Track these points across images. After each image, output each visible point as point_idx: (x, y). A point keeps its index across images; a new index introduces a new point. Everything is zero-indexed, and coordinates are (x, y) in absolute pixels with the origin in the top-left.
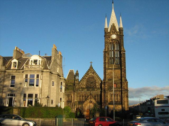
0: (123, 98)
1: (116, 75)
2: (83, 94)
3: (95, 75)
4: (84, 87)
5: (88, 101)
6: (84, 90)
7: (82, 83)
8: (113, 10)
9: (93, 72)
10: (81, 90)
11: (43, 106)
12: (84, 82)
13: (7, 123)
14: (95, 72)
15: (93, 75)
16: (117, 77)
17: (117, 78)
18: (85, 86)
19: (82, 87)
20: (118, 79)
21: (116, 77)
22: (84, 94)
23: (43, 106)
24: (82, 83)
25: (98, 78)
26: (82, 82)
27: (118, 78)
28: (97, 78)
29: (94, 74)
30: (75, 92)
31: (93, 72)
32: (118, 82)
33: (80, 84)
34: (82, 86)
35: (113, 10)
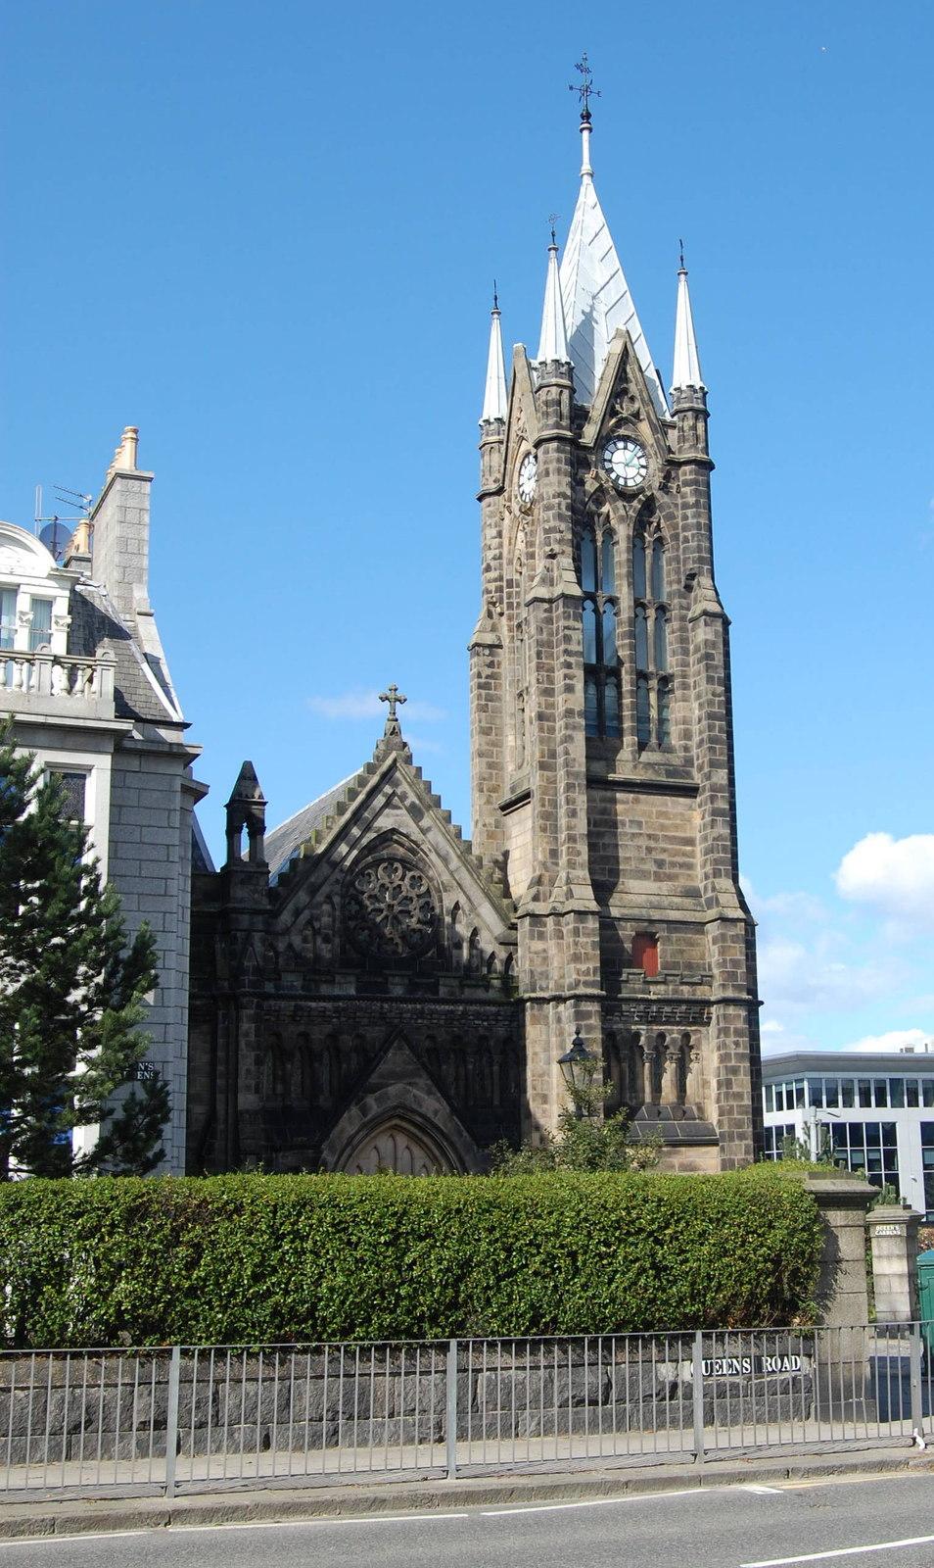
0: (740, 1057)
1: (649, 850)
2: (318, 1033)
3: (436, 837)
4: (326, 950)
5: (370, 1100)
6: (325, 990)
7: (297, 913)
8: (588, 194)
9: (412, 798)
10: (293, 980)
11: (72, 990)
12: (319, 898)
13: (188, 749)
14: (437, 801)
15: (416, 835)
16: (660, 864)
17: (658, 878)
18: (327, 940)
19: (297, 957)
20: (665, 887)
21: (651, 867)
22: (328, 1029)
23: (72, 990)
24: (305, 916)
25: (465, 863)
26: (302, 897)
27: (670, 878)
28: (455, 863)
29: (426, 822)
30: (239, 1007)
31: (412, 798)
32: (420, 1119)
33: (286, 917)
34: (297, 940)
35: (588, 194)
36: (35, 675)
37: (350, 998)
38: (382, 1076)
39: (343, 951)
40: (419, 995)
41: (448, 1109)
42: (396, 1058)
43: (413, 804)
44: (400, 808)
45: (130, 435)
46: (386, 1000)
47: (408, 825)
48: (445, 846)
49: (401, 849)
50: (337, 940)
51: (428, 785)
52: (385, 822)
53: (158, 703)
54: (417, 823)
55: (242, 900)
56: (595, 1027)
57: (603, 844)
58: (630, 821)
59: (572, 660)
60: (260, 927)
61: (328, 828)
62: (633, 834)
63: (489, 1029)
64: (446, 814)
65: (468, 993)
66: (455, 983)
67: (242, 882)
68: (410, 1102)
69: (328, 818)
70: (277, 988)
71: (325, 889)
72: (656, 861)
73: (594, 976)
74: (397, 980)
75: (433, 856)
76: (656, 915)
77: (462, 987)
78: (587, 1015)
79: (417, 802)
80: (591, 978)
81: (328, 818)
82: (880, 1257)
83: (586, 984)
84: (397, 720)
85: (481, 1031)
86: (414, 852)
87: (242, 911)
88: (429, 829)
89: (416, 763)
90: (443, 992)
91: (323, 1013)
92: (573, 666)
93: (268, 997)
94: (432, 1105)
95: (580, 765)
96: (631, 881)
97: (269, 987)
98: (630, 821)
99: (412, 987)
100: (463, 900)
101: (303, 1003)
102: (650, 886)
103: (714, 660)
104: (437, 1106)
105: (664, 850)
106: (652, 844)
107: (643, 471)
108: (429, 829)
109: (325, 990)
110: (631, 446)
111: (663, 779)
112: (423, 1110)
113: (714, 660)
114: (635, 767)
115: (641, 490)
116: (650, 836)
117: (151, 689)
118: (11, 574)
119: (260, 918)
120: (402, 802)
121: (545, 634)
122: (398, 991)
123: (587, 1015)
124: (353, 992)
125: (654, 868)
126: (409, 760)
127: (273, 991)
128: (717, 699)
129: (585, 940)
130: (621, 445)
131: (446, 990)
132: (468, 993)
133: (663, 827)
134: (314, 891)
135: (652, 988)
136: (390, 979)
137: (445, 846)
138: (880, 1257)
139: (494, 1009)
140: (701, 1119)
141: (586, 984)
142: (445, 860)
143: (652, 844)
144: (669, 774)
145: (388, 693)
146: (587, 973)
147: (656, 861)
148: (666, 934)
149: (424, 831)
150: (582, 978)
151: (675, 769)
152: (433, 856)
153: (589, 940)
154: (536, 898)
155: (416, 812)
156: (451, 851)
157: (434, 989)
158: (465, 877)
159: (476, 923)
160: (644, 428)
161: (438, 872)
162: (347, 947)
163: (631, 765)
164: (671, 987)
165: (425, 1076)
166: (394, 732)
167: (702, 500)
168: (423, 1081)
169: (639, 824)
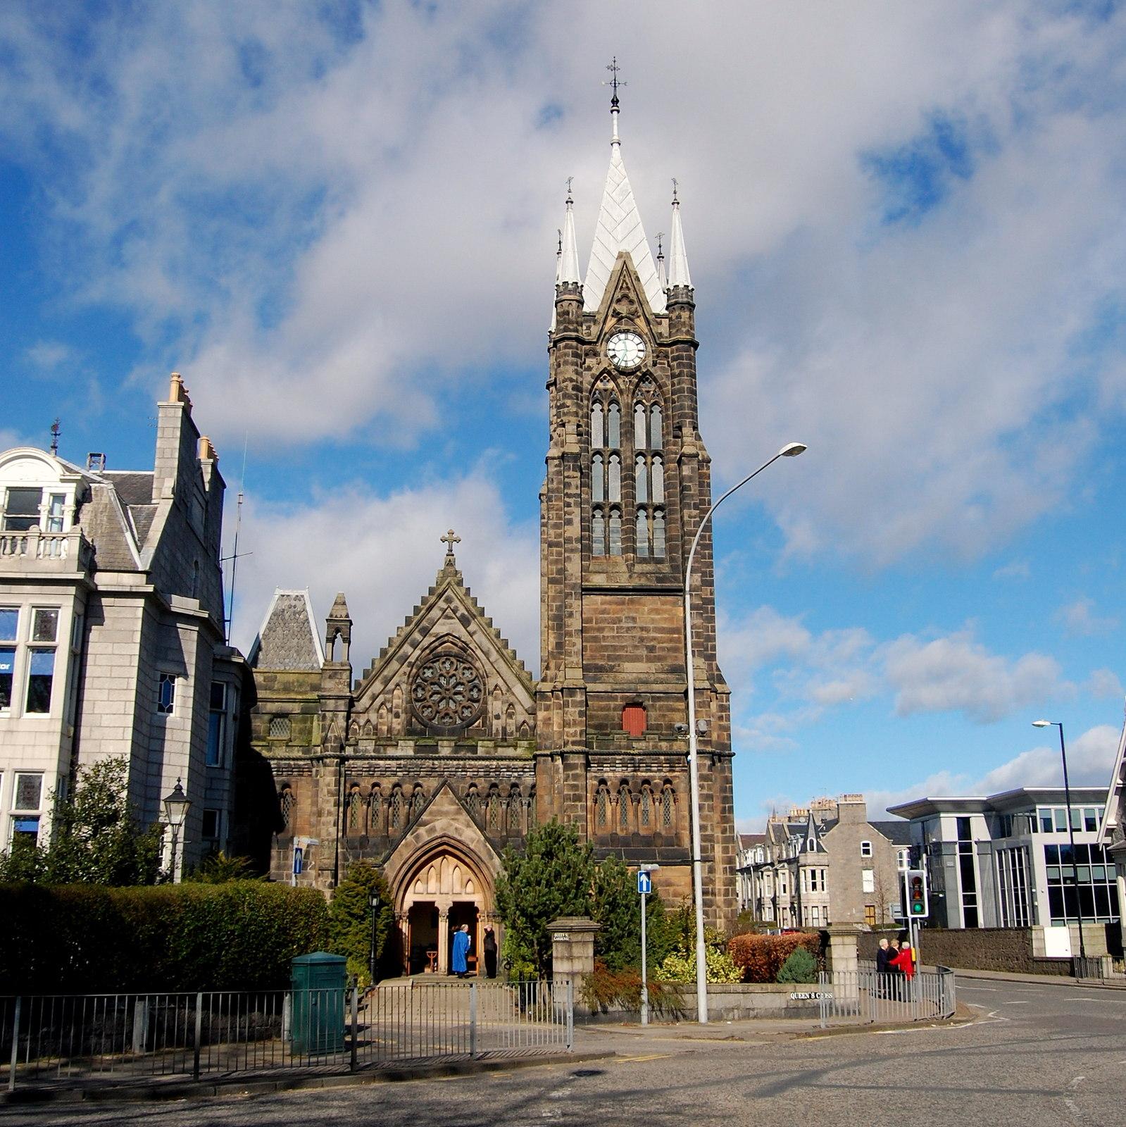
1: (642, 639)
3: (479, 637)
7: (374, 698)
12: (391, 686)
15: (466, 637)
17: (649, 660)
20: (653, 667)
26: (377, 686)
28: (494, 656)
29: (473, 627)
31: (462, 610)
34: (373, 717)
36: (48, 547)
37: (411, 758)
38: (431, 813)
39: (410, 723)
40: (461, 754)
41: (483, 838)
42: (444, 803)
43: (463, 615)
44: (453, 618)
45: (175, 378)
46: (436, 759)
47: (460, 630)
48: (487, 645)
49: (455, 648)
50: (403, 716)
51: (475, 601)
52: (440, 629)
53: (132, 558)
54: (465, 628)
55: (330, 690)
56: (581, 775)
57: (604, 636)
58: (626, 617)
59: (571, 500)
60: (343, 708)
61: (398, 635)
62: (628, 628)
63: (519, 777)
64: (489, 621)
65: (501, 752)
66: (491, 744)
67: (330, 677)
68: (452, 833)
69: (398, 628)
70: (355, 751)
71: (396, 679)
72: (647, 647)
73: (580, 736)
74: (445, 743)
75: (478, 652)
76: (642, 688)
77: (496, 746)
78: (574, 767)
79: (466, 613)
80: (578, 738)
81: (398, 628)
82: (557, 958)
83: (574, 743)
84: (453, 555)
85: (513, 780)
86: (464, 650)
87: (329, 698)
88: (475, 632)
89: (465, 585)
90: (481, 752)
91: (387, 769)
92: (572, 505)
93: (347, 758)
94: (471, 835)
95: (576, 578)
96: (626, 663)
97: (349, 751)
98: (626, 617)
99: (457, 748)
100: (500, 683)
101: (373, 762)
102: (642, 667)
103: (690, 490)
104: (474, 835)
105: (654, 639)
106: (645, 634)
107: (641, 355)
108: (475, 632)
109: (391, 752)
110: (630, 336)
111: (654, 584)
112: (462, 838)
113: (690, 490)
114: (630, 577)
115: (638, 368)
116: (642, 629)
117: (129, 549)
118: (37, 480)
119: (342, 702)
120: (455, 614)
121: (555, 483)
122: (445, 751)
123: (574, 767)
124: (411, 753)
125: (645, 653)
126: (460, 583)
127: (352, 753)
128: (693, 520)
129: (573, 710)
130: (622, 336)
131: (483, 749)
132: (501, 752)
133: (653, 621)
134: (386, 682)
135: (635, 745)
136: (440, 743)
137: (487, 645)
138: (557, 958)
139: (521, 763)
140: (678, 845)
141: (574, 743)
142: (487, 654)
143: (645, 634)
144: (659, 580)
145: (447, 536)
146: (575, 734)
147: (647, 647)
148: (651, 703)
149: (471, 635)
150: (571, 739)
151: (664, 576)
152: (478, 652)
153: (577, 710)
154: (544, 680)
155: (465, 621)
156: (492, 647)
157: (474, 749)
158: (502, 666)
159: (512, 699)
160: (641, 322)
161: (482, 663)
162: (414, 720)
163: (628, 575)
164: (651, 744)
165: (465, 813)
166: (450, 564)
167: (685, 370)
168: (464, 817)
169: (634, 619)
